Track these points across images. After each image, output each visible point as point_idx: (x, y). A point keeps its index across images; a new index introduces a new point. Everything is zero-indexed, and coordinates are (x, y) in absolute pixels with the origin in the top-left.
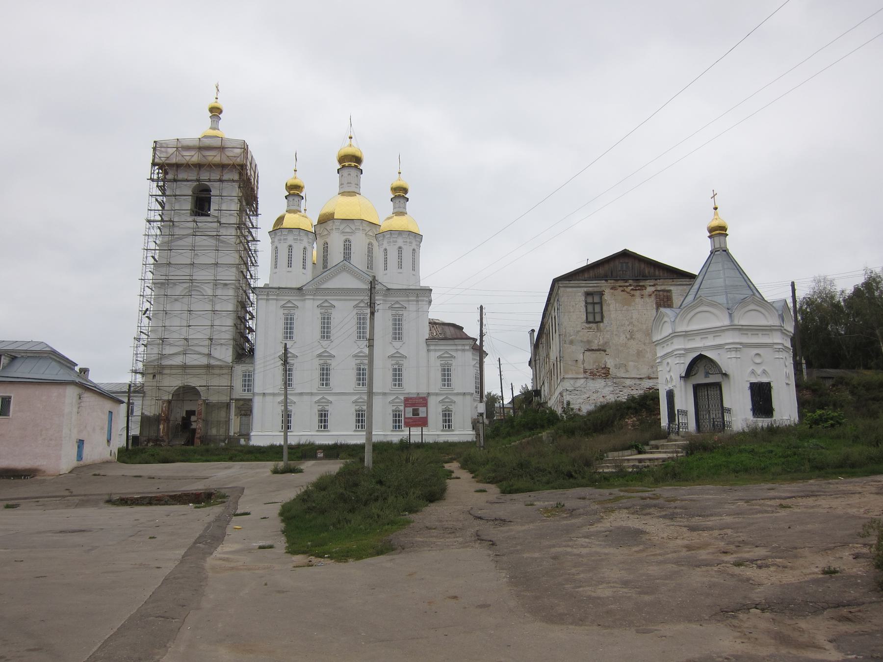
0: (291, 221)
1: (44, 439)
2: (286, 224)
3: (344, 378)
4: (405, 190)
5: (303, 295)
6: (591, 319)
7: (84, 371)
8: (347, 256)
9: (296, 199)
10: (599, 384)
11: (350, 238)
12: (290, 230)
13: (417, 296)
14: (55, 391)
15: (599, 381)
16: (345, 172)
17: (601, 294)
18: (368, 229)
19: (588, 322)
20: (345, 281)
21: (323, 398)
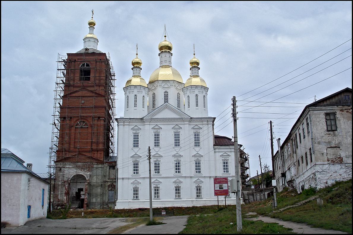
0: (136, 81)
1: (10, 205)
2: (133, 83)
3: (188, 168)
4: (198, 64)
5: (144, 122)
6: (329, 129)
7: (30, 165)
8: (166, 100)
9: (138, 69)
10: (337, 167)
11: (168, 91)
12: (135, 86)
13: (208, 122)
14: (15, 177)
15: (337, 165)
16: (163, 55)
17: (334, 114)
18: (177, 85)
19: (328, 131)
20: (166, 114)
21: (156, 180)
